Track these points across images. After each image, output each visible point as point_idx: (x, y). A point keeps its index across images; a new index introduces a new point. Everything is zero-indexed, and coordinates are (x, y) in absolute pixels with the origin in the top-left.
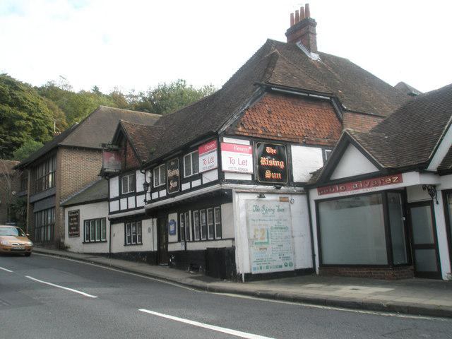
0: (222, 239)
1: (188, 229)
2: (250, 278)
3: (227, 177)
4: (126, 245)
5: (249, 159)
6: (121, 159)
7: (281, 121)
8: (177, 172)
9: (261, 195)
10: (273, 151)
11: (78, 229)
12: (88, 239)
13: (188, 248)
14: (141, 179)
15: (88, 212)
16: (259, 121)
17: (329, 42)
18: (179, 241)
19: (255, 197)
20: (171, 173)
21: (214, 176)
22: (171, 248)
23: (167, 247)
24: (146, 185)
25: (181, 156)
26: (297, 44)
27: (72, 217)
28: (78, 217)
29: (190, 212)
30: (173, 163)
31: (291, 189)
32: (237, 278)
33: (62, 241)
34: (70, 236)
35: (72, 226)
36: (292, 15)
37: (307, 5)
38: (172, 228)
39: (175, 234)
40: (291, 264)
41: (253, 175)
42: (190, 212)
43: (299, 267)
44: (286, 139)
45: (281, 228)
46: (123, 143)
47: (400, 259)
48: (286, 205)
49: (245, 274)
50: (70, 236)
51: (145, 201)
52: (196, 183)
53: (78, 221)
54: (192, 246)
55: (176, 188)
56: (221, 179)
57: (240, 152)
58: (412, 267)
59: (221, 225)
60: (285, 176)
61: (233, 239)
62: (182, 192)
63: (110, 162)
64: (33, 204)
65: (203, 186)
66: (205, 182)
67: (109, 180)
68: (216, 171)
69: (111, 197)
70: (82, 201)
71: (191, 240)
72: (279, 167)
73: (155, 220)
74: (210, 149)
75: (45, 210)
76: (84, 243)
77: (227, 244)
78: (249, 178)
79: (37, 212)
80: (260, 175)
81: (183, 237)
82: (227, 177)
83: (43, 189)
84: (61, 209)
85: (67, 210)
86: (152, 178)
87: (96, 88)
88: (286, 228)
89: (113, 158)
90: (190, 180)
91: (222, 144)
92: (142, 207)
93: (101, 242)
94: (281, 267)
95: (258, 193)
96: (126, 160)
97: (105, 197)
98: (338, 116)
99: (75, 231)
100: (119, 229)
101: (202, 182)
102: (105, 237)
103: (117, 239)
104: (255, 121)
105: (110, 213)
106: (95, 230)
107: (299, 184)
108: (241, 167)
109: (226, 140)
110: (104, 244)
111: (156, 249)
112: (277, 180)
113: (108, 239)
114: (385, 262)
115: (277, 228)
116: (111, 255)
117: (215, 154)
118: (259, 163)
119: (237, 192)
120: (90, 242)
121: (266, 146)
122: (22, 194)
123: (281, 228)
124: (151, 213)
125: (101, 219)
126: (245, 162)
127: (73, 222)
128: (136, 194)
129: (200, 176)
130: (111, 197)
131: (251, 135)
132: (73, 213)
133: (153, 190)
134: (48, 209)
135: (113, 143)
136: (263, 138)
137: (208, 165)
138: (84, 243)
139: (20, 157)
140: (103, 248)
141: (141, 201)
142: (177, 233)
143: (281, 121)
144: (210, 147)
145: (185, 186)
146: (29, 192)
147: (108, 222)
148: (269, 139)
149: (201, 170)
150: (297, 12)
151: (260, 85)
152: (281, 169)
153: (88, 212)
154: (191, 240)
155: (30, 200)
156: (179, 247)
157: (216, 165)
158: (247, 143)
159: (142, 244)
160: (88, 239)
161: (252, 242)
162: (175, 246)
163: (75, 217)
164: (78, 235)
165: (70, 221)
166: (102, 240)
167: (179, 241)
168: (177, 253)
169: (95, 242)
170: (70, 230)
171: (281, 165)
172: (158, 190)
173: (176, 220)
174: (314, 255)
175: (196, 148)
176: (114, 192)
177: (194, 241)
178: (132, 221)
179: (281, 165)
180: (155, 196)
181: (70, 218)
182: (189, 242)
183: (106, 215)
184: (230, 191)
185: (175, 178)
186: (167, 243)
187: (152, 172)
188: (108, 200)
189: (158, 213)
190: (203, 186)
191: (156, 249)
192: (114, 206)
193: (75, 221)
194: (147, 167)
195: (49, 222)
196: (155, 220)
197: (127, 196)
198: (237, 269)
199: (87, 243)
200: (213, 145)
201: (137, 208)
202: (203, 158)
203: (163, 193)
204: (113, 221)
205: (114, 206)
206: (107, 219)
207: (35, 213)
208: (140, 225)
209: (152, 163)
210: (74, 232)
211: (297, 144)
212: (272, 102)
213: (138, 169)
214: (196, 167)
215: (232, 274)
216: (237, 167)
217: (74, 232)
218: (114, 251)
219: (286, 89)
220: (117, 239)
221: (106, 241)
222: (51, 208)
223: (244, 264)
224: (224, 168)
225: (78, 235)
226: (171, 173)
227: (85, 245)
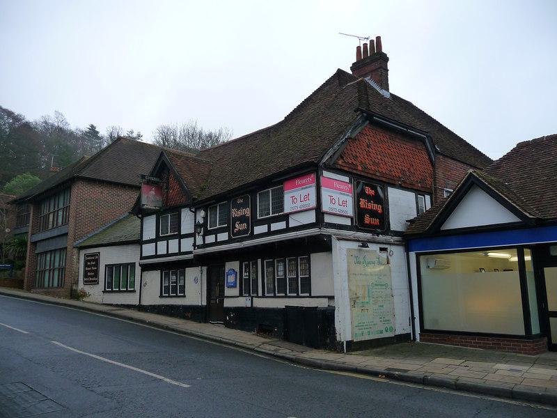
0: (310, 297)
1: (256, 281)
2: (353, 346)
3: (327, 219)
4: (161, 296)
5: (350, 200)
6: (163, 196)
7: (379, 157)
8: (247, 212)
9: (364, 244)
10: (372, 192)
11: (96, 274)
12: (109, 288)
13: (255, 305)
14: (188, 221)
15: (109, 256)
16: (358, 154)
17: (402, 83)
18: (241, 295)
19: (355, 245)
20: (235, 213)
21: (311, 218)
22: (228, 303)
23: (222, 302)
24: (197, 226)
25: (253, 193)
26: (367, 79)
27: (90, 261)
28: (97, 262)
29: (259, 261)
30: (240, 201)
31: (388, 238)
32: (335, 346)
33: (74, 288)
34: (86, 283)
35: (89, 271)
36: (359, 48)
37: (378, 39)
38: (231, 279)
39: (236, 287)
40: (392, 329)
41: (352, 219)
42: (259, 261)
43: (398, 333)
44: (384, 179)
45: (382, 285)
46: (165, 176)
47: (536, 329)
48: (384, 255)
49: (348, 342)
50: (86, 283)
51: (194, 245)
52: (276, 226)
53: (97, 265)
54: (260, 303)
55: (245, 231)
56: (319, 222)
57: (340, 190)
58: (546, 339)
59: (309, 279)
60: (382, 225)
61: (331, 298)
62: (253, 236)
63: (150, 198)
64: (35, 244)
65: (288, 230)
66: (291, 225)
67: (142, 219)
68: (314, 213)
69: (145, 238)
70: (105, 242)
71: (260, 294)
72: (377, 211)
73: (205, 269)
74: (303, 185)
75: (51, 251)
76: (105, 292)
77: (323, 303)
78: (348, 222)
79: (41, 253)
80: (359, 222)
81: (247, 288)
82: (327, 219)
83: (50, 226)
84: (75, 251)
85: (83, 253)
86: (205, 218)
87: (92, 126)
88: (386, 285)
89: (153, 192)
90: (269, 221)
91: (321, 178)
92: (191, 252)
93: (127, 291)
94: (381, 332)
95: (359, 241)
96: (167, 196)
97: (136, 237)
98: (430, 158)
99: (92, 277)
100: (154, 278)
101: (287, 224)
102: (133, 285)
103: (151, 289)
104: (354, 154)
105: (142, 258)
106: (120, 276)
107: (396, 233)
108: (342, 208)
109: (326, 174)
110: (132, 294)
111: (204, 303)
112: (375, 226)
113: (137, 287)
114: (523, 333)
115: (376, 285)
116: (141, 308)
117: (312, 191)
118: (359, 205)
119: (339, 239)
120: (112, 292)
121: (367, 185)
122: (18, 232)
123: (382, 285)
124: (198, 261)
125: (128, 264)
126: (344, 203)
127: (88, 266)
128: (180, 237)
129: (286, 218)
130: (145, 238)
131: (350, 170)
132: (91, 256)
133: (207, 233)
134: (55, 250)
135: (152, 174)
136: (361, 176)
137: (299, 204)
138: (105, 292)
139: (10, 191)
140: (132, 299)
141: (187, 245)
142: (238, 286)
143: (379, 157)
144: (304, 181)
145: (258, 230)
146: (30, 230)
147: (138, 269)
148: (369, 178)
149: (287, 210)
150: (365, 45)
151: (362, 112)
152: (379, 213)
153: (109, 256)
154: (260, 294)
155: (30, 239)
156: (243, 302)
157: (313, 204)
158: (346, 179)
159: (184, 296)
160: (109, 288)
161: (354, 301)
162: (234, 299)
163: (93, 262)
164: (96, 282)
165: (86, 265)
166: (179, 294)
167: (241, 295)
168: (239, 311)
169: (120, 291)
170: (86, 275)
171: (378, 208)
172: (216, 232)
173: (238, 271)
174: (413, 318)
175: (281, 182)
176: (150, 231)
177: (264, 296)
178: (172, 268)
179: (378, 208)
180: (210, 239)
181: (86, 262)
182: (258, 297)
183: (137, 260)
184: (329, 237)
185: (243, 219)
186: (222, 296)
187: (206, 211)
188: (140, 242)
189: (213, 263)
190: (288, 230)
191: (204, 303)
192: (148, 250)
193: (94, 266)
194: (195, 206)
195: (57, 265)
196: (205, 269)
197: (167, 238)
198: (338, 336)
199: (124, 291)
200: (309, 179)
201: (180, 253)
202: (291, 195)
203: (223, 237)
204: (145, 268)
205: (148, 250)
206: (137, 265)
207: (38, 254)
208: (183, 274)
209: (207, 200)
210: (91, 277)
211: (393, 186)
212: (371, 134)
213: (185, 206)
214: (279, 205)
215: (328, 341)
216: (337, 208)
217: (91, 277)
218: (145, 302)
219: (386, 120)
220: (151, 289)
221: (134, 291)
222: (60, 249)
223: (345, 329)
224: (325, 208)
225: (96, 282)
226: (235, 213)
227: (106, 295)
